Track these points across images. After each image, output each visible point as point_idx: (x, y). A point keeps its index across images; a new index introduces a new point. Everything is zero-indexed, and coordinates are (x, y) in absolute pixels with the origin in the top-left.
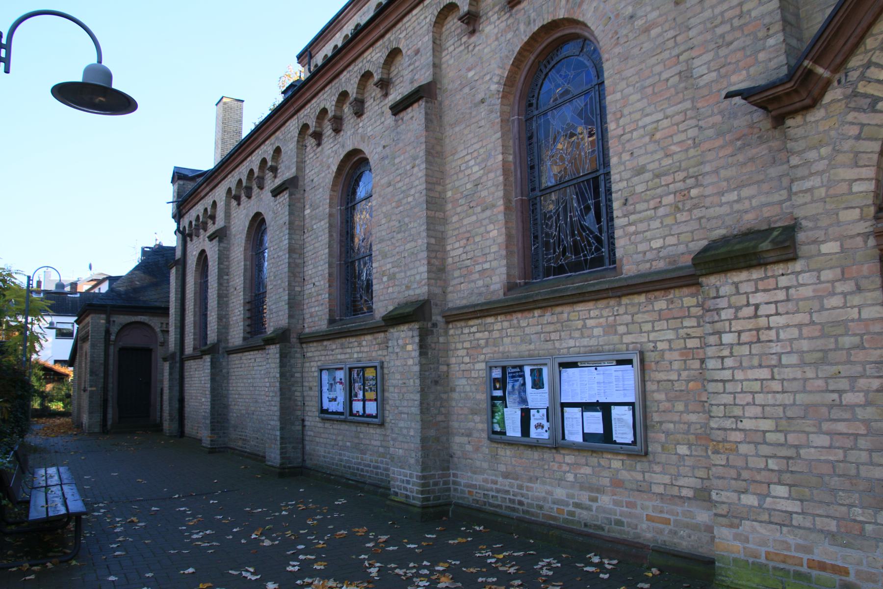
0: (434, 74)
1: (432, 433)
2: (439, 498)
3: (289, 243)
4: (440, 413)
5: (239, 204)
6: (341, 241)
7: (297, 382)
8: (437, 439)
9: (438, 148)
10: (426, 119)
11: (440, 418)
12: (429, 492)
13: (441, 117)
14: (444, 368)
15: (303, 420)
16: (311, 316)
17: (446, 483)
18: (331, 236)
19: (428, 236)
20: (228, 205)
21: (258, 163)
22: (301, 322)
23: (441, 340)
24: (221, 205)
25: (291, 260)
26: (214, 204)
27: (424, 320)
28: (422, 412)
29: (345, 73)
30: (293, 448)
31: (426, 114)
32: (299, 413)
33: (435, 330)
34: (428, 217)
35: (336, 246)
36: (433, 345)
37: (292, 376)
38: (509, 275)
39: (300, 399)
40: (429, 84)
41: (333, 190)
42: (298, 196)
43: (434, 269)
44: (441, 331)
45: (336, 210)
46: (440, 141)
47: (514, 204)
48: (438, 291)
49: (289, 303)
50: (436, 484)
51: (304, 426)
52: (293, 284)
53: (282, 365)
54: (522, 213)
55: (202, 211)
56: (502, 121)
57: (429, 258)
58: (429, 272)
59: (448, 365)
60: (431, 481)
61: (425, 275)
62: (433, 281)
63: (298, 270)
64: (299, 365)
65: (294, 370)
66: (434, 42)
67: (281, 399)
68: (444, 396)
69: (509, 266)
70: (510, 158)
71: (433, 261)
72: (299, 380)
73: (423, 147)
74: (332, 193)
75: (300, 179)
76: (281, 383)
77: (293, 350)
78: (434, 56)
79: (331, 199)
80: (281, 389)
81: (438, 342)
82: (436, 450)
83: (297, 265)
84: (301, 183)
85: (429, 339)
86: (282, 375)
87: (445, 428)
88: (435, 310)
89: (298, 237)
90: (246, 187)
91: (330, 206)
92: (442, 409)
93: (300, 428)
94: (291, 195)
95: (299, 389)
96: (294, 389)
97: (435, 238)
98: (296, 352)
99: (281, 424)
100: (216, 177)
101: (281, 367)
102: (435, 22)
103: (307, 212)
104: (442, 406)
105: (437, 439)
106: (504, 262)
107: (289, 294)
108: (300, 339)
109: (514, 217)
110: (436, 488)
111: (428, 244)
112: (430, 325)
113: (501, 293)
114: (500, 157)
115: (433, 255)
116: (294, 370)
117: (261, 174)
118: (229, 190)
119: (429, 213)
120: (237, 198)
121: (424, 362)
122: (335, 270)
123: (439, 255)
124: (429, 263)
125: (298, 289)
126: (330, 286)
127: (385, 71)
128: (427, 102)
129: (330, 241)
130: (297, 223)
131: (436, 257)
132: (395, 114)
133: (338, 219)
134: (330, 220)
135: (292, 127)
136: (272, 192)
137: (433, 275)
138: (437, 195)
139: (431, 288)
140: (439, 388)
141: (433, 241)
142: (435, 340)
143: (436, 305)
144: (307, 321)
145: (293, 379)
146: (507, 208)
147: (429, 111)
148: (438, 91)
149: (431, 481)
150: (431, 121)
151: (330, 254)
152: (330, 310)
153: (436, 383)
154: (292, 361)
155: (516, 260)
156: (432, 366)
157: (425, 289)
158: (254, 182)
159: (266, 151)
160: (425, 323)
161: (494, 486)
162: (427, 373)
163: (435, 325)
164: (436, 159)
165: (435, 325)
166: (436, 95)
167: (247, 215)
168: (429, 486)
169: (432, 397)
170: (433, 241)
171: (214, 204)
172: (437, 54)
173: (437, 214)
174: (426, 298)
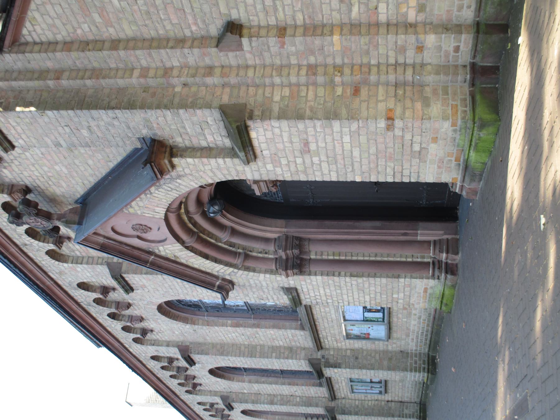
0: (173, 346)
1: (385, 363)
2: (424, 361)
3: (267, 404)
4: (374, 357)
5: (201, 385)
6: (267, 376)
7: (362, 404)
8: (390, 359)
9: (219, 347)
10: (201, 354)
11: (377, 357)
12: (420, 368)
13: (199, 344)
14: (349, 352)
15: (388, 401)
16: (317, 393)
17: (416, 356)
18: (264, 383)
19: (271, 358)
20: (155, 343)
21: (164, 372)
22: (321, 399)
23: (332, 353)
24: (199, 398)
25: (279, 403)
26: (155, 358)
27: (320, 364)
28: (373, 369)
29: (158, 375)
30: (407, 408)
31: (198, 354)
32: (383, 403)
33: (326, 357)
34: (260, 357)
35: (270, 379)
36: (335, 359)
37: (358, 406)
38: (296, 329)
39: (373, 402)
40: (180, 351)
41: (233, 380)
42: (234, 396)
43: (290, 355)
44: (327, 352)
45: (246, 378)
46: (214, 345)
47: (256, 322)
48: (303, 354)
49: (308, 406)
50: (416, 363)
51: (392, 401)
52: (295, 402)
53: (350, 413)
54: (261, 319)
55: (200, 406)
56: (208, 325)
57: (284, 358)
58: (292, 359)
59: (347, 349)
60: (414, 365)
61: (294, 361)
62: (298, 356)
63: (285, 398)
64: (350, 401)
65: (353, 405)
66: (153, 345)
67: (373, 415)
68: (365, 353)
69: (291, 328)
70: (229, 322)
71: (286, 356)
72: (360, 402)
73: (218, 357)
74: (235, 380)
75: (222, 394)
76: (361, 415)
77: (339, 405)
78: (162, 345)
79: (239, 381)
80: (366, 415)
81: (333, 355)
82: (397, 361)
83: (282, 399)
84: (225, 394)
85: (331, 361)
86: (356, 414)
87: (383, 354)
88: (315, 356)
89: (262, 397)
90: (117, 308)
91: (244, 382)
92: (373, 355)
93: (393, 403)
94: (233, 401)
95: (367, 402)
96: (366, 406)
97: (272, 352)
98: (341, 403)
99: (389, 416)
100: (189, 414)
101: (351, 414)
102: (141, 344)
103: (245, 391)
104: (371, 355)
105: (390, 359)
106: (288, 330)
107: (302, 406)
108: (332, 400)
109: (263, 323)
110: (418, 362)
111: (276, 358)
112: (323, 360)
113: (305, 332)
114: (229, 328)
115: (282, 355)
116: (353, 405)
117: (114, 305)
118: (136, 340)
119: (257, 356)
120: (195, 386)
121: (344, 366)
122: (287, 380)
123: (282, 351)
124: (287, 358)
125: (298, 399)
126: (297, 385)
127: (163, 360)
128: (191, 353)
129: (267, 383)
130: (253, 398)
131: (284, 353)
132: (195, 364)
133: (253, 378)
134: (253, 383)
135: (136, 349)
136: (230, 410)
137: (294, 356)
138: (247, 350)
139: (302, 357)
140: (360, 357)
141: (274, 355)
142: (332, 357)
143: (312, 355)
144: (320, 395)
145: (360, 406)
146: (258, 326)
147: (197, 352)
148: (184, 344)
149: (414, 365)
150: (203, 351)
151: (276, 383)
152: (313, 386)
153: (357, 358)
154: (347, 406)
155: (287, 323)
156: (347, 360)
157: (303, 362)
158: (123, 313)
159: (155, 366)
160: (322, 363)
161: (415, 340)
162: (351, 364)
163: (323, 357)
164: (225, 349)
165: (323, 357)
166: (186, 346)
167: (242, 417)
168: (416, 367)
169: (365, 362)
170: (274, 355)
171: (155, 358)
172: (160, 343)
173: (258, 350)
174: (307, 362)
